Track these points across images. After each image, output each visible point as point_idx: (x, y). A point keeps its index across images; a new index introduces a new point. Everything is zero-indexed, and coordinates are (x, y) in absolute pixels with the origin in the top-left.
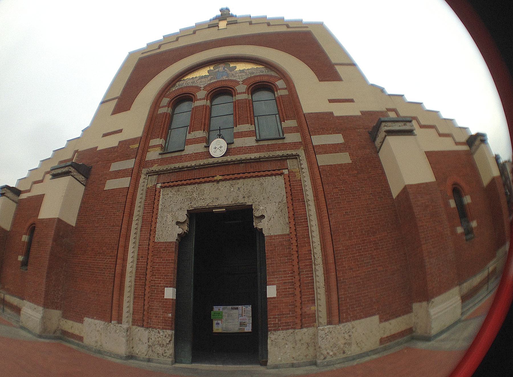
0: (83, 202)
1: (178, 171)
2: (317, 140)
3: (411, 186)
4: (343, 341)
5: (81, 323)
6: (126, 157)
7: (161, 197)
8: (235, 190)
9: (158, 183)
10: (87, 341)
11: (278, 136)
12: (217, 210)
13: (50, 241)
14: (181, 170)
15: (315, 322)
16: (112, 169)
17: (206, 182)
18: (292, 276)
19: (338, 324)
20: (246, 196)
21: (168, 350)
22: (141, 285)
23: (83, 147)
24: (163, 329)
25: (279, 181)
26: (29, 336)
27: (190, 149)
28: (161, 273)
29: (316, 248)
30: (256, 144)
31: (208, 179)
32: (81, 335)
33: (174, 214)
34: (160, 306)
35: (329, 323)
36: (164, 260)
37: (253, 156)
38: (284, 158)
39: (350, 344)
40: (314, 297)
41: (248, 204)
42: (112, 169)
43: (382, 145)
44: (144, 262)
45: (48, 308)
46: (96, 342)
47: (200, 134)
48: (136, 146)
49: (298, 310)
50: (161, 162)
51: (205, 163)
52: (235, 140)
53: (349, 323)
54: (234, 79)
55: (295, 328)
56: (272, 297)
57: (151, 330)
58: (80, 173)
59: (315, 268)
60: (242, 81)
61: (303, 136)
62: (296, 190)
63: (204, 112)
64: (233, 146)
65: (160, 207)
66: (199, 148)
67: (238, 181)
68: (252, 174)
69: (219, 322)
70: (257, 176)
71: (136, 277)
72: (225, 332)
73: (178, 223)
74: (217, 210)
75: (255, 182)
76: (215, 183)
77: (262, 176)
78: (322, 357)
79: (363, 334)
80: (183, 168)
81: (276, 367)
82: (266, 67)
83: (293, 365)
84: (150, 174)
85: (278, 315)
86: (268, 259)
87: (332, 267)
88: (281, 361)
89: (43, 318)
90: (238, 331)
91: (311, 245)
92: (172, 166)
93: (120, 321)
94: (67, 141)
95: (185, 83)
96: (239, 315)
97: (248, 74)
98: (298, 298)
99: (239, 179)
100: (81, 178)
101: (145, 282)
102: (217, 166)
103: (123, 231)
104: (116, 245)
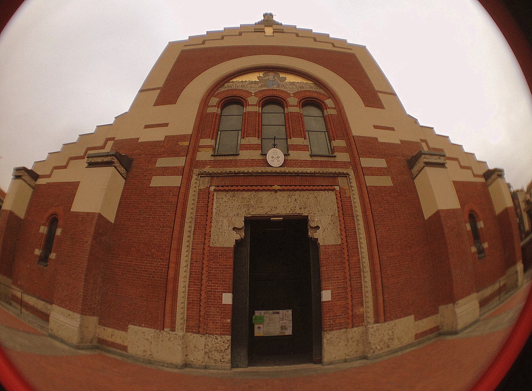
0: (123, 198)
1: (233, 176)
2: (366, 162)
3: (443, 210)
4: (388, 337)
5: (124, 330)
6: (176, 154)
7: (215, 200)
8: (293, 201)
9: (212, 186)
10: (131, 351)
11: (327, 154)
12: (274, 219)
13: (89, 239)
14: (236, 175)
15: (364, 321)
16: (158, 165)
18: (344, 282)
19: (384, 323)
20: (302, 207)
21: (226, 355)
22: (195, 290)
23: (121, 136)
24: (221, 334)
25: (330, 197)
26: (66, 347)
27: (245, 155)
28: (218, 278)
29: (364, 258)
30: (310, 159)
31: (266, 188)
32: (126, 344)
33: (230, 219)
34: (218, 312)
35: (377, 321)
36: (220, 265)
37: (309, 170)
39: (393, 339)
40: (362, 300)
41: (304, 215)
42: (158, 165)
43: (418, 174)
44: (200, 267)
45: (86, 315)
46: (145, 351)
47: (255, 141)
48: (187, 143)
49: (350, 312)
50: (214, 164)
51: (264, 171)
52: (241, 152)
53: (392, 322)
54: (285, 90)
55: (347, 328)
56: (327, 300)
57: (207, 336)
58: (122, 165)
59: (364, 275)
60: (293, 94)
61: (352, 157)
62: (347, 206)
63: (257, 118)
64: (289, 158)
65: (214, 211)
66: (256, 155)
67: (295, 193)
68: (307, 187)
69: (261, 326)
70: (312, 190)
71: (190, 282)
72: (266, 335)
73: (234, 229)
74: (274, 219)
75: (311, 195)
76: (273, 193)
77: (316, 190)
78: (372, 351)
79: (403, 330)
80: (239, 173)
81: (331, 363)
82: (315, 83)
83: (345, 361)
84: (202, 175)
85: (333, 316)
86: (323, 266)
87: (379, 274)
88: (335, 357)
89: (81, 326)
90: (281, 335)
91: (360, 255)
92: (228, 170)
93: (173, 329)
94: (97, 126)
95: (234, 85)
96: (280, 319)
97: (298, 88)
99: (296, 190)
100: (123, 170)
101: (201, 287)
102: (275, 176)
103: (176, 234)
104: (168, 247)
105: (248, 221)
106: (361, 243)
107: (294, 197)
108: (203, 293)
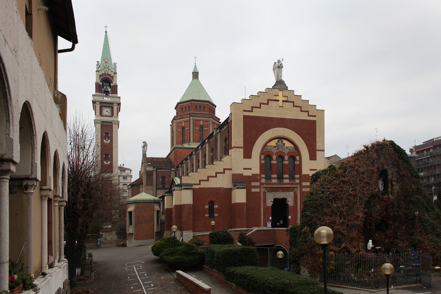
17: (278, 192)
73: (272, 202)
82: (295, 147)
99: (284, 191)
105: (274, 199)
106: (298, 206)
108: (266, 217)
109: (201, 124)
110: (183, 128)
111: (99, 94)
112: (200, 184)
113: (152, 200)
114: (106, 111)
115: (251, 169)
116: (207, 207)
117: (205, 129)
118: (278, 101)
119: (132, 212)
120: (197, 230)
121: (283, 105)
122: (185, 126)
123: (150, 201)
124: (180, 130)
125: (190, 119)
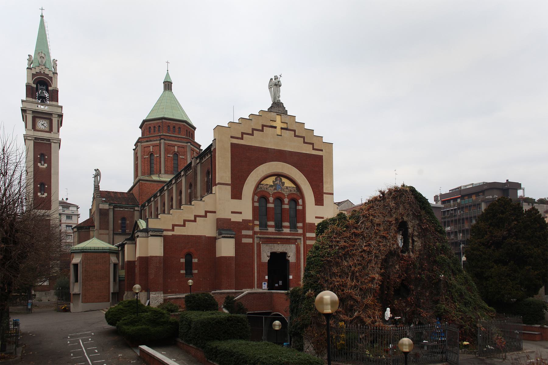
17: (275, 244)
30: (290, 232)
38: (297, 239)
61: (304, 231)
73: (268, 256)
82: (296, 188)
98: (297, 279)
99: (284, 244)
105: (271, 253)
107: (284, 246)
109: (176, 151)
110: (151, 154)
111: (31, 99)
112: (173, 230)
113: (106, 250)
114: (42, 124)
115: (241, 213)
116: (183, 260)
117: (181, 157)
118: (275, 127)
119: (78, 264)
120: (169, 292)
121: (281, 133)
122: (153, 152)
123: (104, 251)
124: (147, 157)
125: (160, 143)
